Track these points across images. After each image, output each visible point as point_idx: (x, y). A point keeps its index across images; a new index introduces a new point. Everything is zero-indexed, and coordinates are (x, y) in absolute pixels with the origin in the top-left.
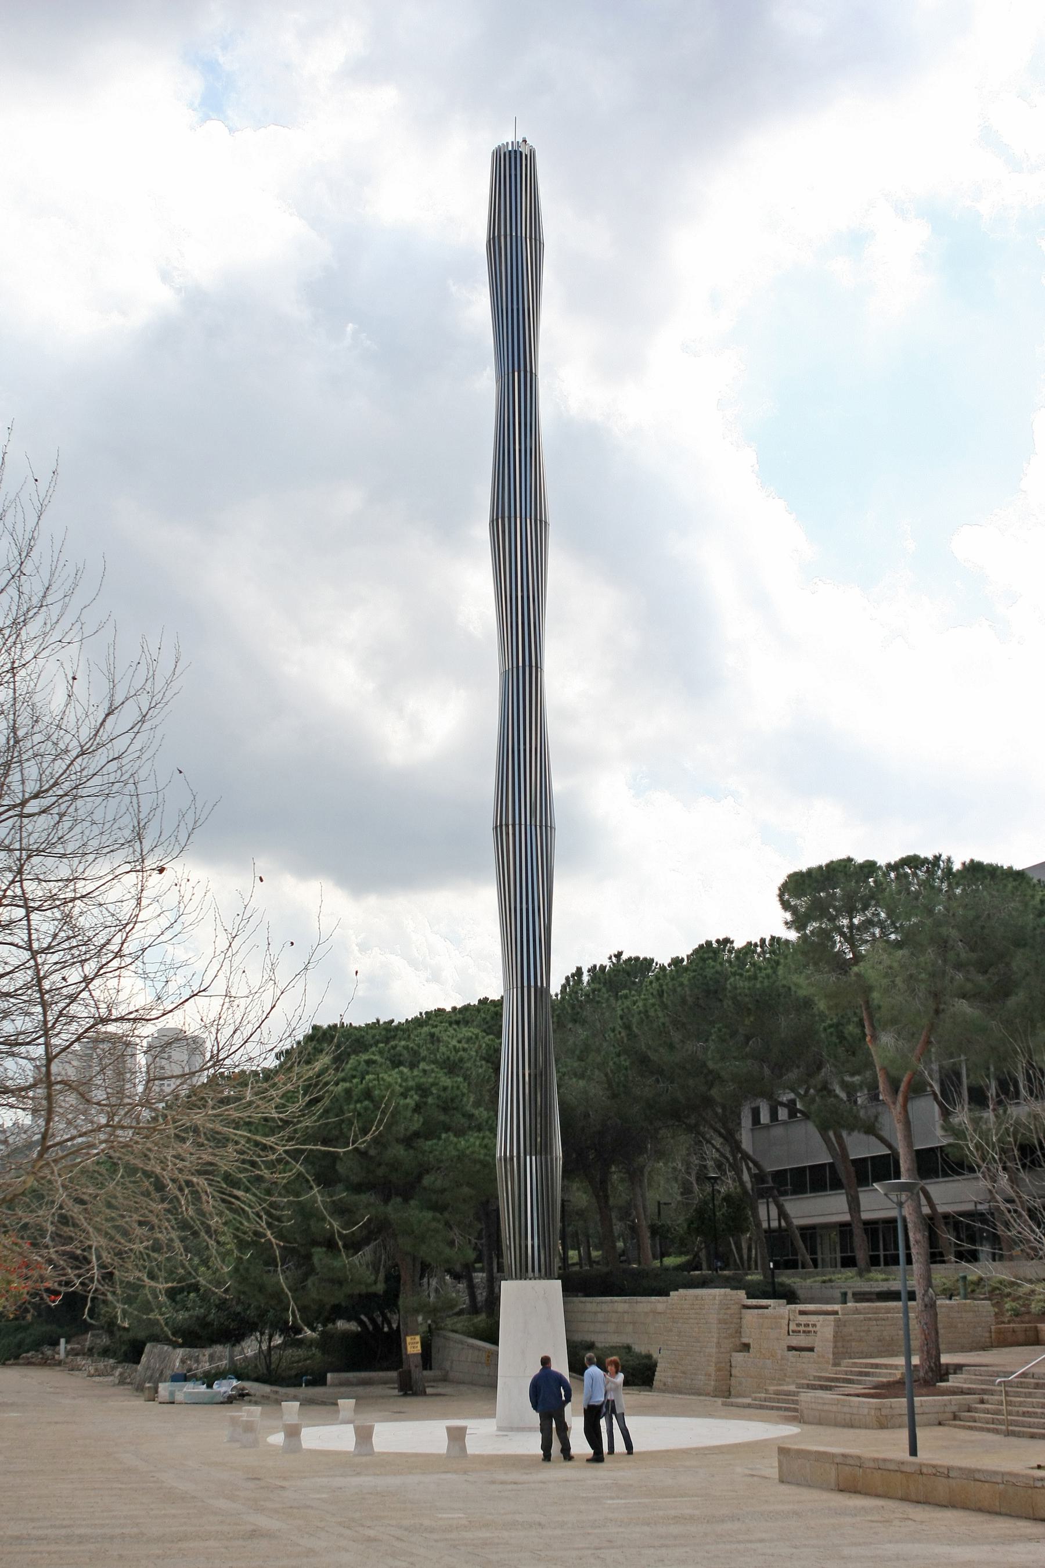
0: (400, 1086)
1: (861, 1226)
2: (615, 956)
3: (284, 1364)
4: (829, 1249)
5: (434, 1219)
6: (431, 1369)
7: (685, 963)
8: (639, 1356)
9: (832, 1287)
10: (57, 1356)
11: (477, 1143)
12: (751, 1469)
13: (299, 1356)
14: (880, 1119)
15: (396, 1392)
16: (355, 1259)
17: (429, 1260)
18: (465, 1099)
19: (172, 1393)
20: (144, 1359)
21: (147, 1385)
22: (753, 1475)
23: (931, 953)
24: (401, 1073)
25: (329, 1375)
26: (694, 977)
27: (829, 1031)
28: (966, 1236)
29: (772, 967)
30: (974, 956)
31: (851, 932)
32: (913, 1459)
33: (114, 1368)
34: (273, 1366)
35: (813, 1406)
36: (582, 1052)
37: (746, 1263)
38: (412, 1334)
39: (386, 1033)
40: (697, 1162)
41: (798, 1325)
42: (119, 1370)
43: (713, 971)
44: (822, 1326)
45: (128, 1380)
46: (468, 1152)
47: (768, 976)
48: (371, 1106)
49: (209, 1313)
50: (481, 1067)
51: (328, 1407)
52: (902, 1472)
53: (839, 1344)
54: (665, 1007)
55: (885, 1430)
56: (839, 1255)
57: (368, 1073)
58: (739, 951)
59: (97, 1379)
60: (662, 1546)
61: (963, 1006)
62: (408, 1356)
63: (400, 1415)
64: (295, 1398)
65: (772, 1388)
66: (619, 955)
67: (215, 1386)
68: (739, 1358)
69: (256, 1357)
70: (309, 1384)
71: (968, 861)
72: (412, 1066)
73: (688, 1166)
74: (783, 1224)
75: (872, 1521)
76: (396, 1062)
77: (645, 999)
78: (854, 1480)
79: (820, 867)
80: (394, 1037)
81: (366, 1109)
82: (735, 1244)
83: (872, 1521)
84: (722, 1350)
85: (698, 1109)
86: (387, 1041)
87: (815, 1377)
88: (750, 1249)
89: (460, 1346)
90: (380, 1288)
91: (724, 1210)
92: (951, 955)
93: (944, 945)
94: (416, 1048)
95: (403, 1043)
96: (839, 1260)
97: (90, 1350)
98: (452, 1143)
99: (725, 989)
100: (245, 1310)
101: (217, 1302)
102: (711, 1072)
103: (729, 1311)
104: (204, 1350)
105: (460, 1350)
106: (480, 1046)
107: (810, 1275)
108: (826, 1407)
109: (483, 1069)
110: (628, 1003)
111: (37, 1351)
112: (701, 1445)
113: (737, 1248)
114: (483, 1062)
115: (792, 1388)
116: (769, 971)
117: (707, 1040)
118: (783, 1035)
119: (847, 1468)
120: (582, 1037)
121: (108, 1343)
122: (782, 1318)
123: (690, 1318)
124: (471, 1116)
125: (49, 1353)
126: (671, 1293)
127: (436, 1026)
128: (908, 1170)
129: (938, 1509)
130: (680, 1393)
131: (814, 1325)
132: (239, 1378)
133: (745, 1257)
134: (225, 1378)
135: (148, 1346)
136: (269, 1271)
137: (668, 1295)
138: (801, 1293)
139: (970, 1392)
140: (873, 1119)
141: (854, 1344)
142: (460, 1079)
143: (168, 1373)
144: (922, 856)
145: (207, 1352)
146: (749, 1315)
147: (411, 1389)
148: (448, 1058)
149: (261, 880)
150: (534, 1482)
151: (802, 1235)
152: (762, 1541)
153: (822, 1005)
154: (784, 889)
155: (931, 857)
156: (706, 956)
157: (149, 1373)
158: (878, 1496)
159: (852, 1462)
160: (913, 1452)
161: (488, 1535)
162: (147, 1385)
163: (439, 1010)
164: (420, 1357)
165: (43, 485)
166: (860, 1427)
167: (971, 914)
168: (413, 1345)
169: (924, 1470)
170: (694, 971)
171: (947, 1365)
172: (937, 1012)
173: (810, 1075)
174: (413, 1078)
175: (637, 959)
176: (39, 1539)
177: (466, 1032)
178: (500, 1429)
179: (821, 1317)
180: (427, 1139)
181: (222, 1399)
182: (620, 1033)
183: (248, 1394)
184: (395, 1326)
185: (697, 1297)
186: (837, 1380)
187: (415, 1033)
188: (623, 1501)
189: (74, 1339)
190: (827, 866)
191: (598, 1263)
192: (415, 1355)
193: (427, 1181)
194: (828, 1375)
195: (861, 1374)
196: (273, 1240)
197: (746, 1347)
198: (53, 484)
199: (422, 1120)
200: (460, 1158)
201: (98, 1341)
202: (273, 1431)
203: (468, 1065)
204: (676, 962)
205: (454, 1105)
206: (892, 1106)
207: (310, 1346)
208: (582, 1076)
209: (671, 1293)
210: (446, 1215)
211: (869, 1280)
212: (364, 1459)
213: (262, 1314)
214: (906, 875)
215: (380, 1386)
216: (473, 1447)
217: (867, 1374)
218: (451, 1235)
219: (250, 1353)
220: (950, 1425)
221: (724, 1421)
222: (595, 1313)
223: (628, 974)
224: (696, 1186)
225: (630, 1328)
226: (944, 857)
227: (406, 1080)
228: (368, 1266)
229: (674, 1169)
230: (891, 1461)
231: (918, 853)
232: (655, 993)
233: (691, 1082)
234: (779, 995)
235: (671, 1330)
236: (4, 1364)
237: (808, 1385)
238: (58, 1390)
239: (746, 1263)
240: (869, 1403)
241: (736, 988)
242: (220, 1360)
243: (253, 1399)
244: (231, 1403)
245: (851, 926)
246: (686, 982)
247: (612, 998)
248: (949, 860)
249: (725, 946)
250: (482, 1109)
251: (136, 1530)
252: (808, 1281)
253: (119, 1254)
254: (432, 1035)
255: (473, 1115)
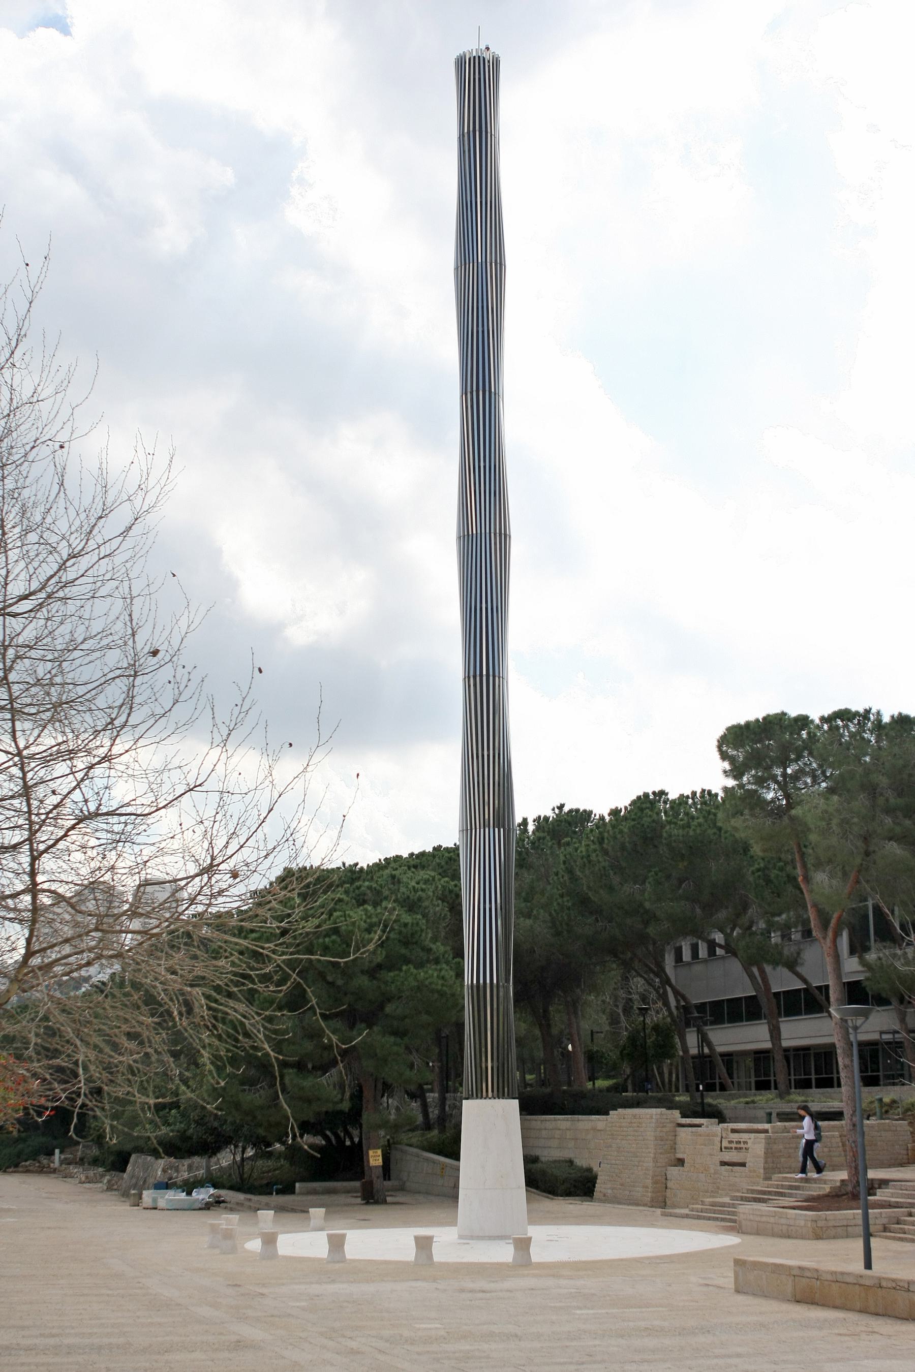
0: (365, 922)
1: (782, 1053)
2: (558, 808)
3: (255, 1175)
4: (745, 1073)
5: (395, 1044)
6: (389, 1179)
7: (622, 813)
8: (581, 1169)
9: (755, 1108)
10: (52, 1165)
11: (435, 975)
12: (705, 1278)
13: (269, 1166)
14: (802, 955)
15: (359, 1200)
16: (323, 1080)
17: (390, 1081)
18: (424, 935)
19: (155, 1200)
20: (129, 1168)
21: (133, 1192)
22: (707, 1285)
23: (861, 801)
24: (366, 910)
25: (297, 1185)
26: (633, 826)
27: (756, 874)
28: (878, 1065)
29: (704, 817)
30: (900, 801)
31: (785, 779)
32: (868, 1272)
33: (102, 1176)
34: (245, 1176)
35: (751, 1217)
36: (527, 894)
37: (667, 1086)
38: (375, 1148)
39: (352, 874)
40: (624, 996)
41: (731, 1142)
42: (108, 1177)
43: (649, 820)
44: (754, 1143)
45: (115, 1187)
46: (427, 983)
47: (700, 825)
48: (338, 940)
49: (189, 1128)
50: (438, 905)
51: (298, 1214)
52: (860, 1285)
53: (769, 1160)
54: (606, 853)
55: (821, 1241)
56: (753, 1080)
57: (335, 910)
58: (673, 801)
59: (87, 1185)
60: (643, 1361)
61: (894, 849)
62: (370, 1168)
63: (365, 1223)
64: (268, 1207)
65: (708, 1200)
66: (561, 807)
67: (194, 1194)
68: (674, 1171)
69: (230, 1167)
70: (279, 1192)
71: (896, 714)
72: (376, 904)
73: (616, 998)
74: (706, 1050)
75: (840, 1335)
76: (361, 902)
77: (588, 845)
78: (811, 1291)
79: (757, 720)
80: (358, 879)
81: (334, 942)
82: (658, 1069)
83: (840, 1335)
84: (659, 1164)
85: (634, 947)
86: (352, 881)
87: (748, 1190)
88: (670, 1074)
89: (416, 1159)
90: (346, 1106)
91: (653, 1038)
92: (881, 801)
93: (872, 791)
94: (378, 888)
95: (367, 883)
96: (753, 1085)
97: (82, 1159)
98: (412, 974)
99: (661, 836)
100: (221, 1125)
101: (197, 1118)
102: (647, 911)
103: (664, 1129)
104: (183, 1161)
105: (418, 1162)
106: (437, 887)
107: (733, 1097)
108: (764, 1219)
109: (440, 908)
110: (570, 849)
111: (34, 1160)
112: (651, 1254)
113: (659, 1073)
114: (440, 902)
115: (727, 1200)
116: (701, 820)
117: (644, 882)
118: (714, 878)
119: (804, 1280)
120: (528, 880)
121: (98, 1153)
122: (716, 1135)
123: (627, 1136)
124: (429, 950)
125: (45, 1162)
126: (611, 1112)
127: (397, 869)
128: (837, 1000)
129: (899, 1322)
130: (620, 1203)
131: (745, 1143)
132: (215, 1186)
133: (667, 1080)
134: (202, 1187)
135: (133, 1157)
136: (245, 1090)
137: (608, 1114)
138: (727, 1113)
139: (897, 1205)
140: (795, 955)
141: (783, 1160)
142: (419, 916)
143: (151, 1181)
144: (853, 710)
145: (186, 1162)
146: (683, 1133)
147: (373, 1198)
148: (408, 897)
149: (260, 671)
150: (501, 1291)
151: (723, 1060)
152: (739, 1355)
153: (757, 849)
154: (723, 742)
155: (861, 711)
156: (644, 806)
157: (134, 1181)
158: (835, 1307)
159: (808, 1274)
160: (868, 1265)
161: (468, 1347)
162: (133, 1192)
163: (397, 856)
164: (381, 1170)
165: (35, 268)
166: (796, 1238)
167: (901, 762)
168: (375, 1158)
169: (884, 1284)
170: (634, 820)
171: (872, 1180)
172: (867, 854)
173: (738, 916)
174: (377, 915)
175: (577, 810)
176: (28, 1349)
177: (423, 874)
178: (461, 1237)
179: (752, 1135)
180: (390, 970)
181: (200, 1206)
182: (563, 877)
183: (223, 1202)
184: (356, 1140)
185: (635, 1116)
186: (769, 1193)
187: (378, 874)
188: (592, 1312)
189: (68, 1150)
190: (764, 719)
191: (531, 1085)
192: (376, 1167)
193: (389, 1009)
194: (759, 1188)
195: (791, 1187)
196: (272, 1053)
197: (681, 1162)
198: (45, 269)
199: (384, 953)
200: (419, 989)
201: (89, 1152)
202: (250, 1237)
203: (426, 903)
204: (615, 812)
205: (414, 940)
206: (822, 941)
207: (279, 1158)
208: (529, 916)
209: (611, 1112)
210: (406, 1039)
211: (789, 1101)
212: (337, 1266)
213: (238, 1129)
214: (838, 727)
215: (344, 1195)
216: (439, 1254)
217: (797, 1188)
218: (411, 1057)
219: (224, 1164)
220: (880, 1237)
221: (667, 1231)
222: (540, 1130)
223: (570, 824)
224: (622, 1018)
225: (571, 1144)
226: (874, 711)
227: (370, 917)
228: (334, 1087)
229: (604, 1002)
230: (849, 1274)
231: (849, 707)
232: (595, 840)
233: (629, 921)
234: (710, 842)
235: (611, 1146)
236: (5, 1171)
237: (742, 1197)
238: (53, 1196)
239: (667, 1086)
240: (806, 1215)
241: (670, 836)
242: (198, 1169)
243: (228, 1205)
244: (209, 1209)
245: (784, 775)
246: (626, 830)
247: (555, 846)
248: (878, 713)
249: (660, 798)
250: (439, 944)
251: (122, 1340)
252: (733, 1102)
253: (108, 1068)
254: (393, 877)
255: (431, 949)
